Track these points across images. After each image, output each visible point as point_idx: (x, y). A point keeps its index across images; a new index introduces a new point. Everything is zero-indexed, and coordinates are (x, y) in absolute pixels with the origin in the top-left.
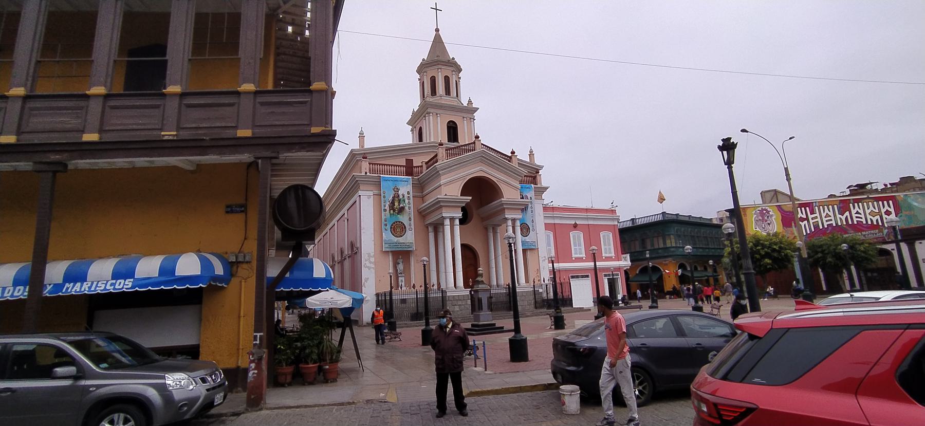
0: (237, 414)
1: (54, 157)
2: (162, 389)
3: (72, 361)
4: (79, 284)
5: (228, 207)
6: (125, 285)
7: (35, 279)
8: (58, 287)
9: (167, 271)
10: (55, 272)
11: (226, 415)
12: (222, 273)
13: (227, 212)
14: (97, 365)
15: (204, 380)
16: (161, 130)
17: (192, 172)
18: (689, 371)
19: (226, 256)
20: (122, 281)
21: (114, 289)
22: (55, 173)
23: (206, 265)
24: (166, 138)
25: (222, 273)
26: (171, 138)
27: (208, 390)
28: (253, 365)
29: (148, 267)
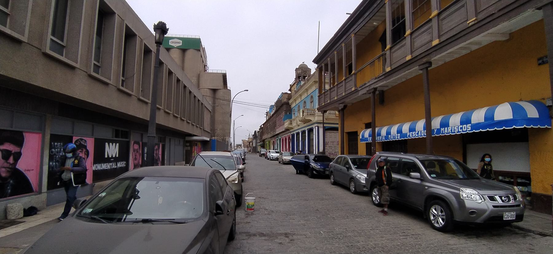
0: (543, 235)
1: (425, 60)
2: (457, 196)
3: (418, 170)
4: (446, 128)
5: (539, 60)
6: (467, 129)
7: (428, 126)
8: (439, 130)
9: (489, 117)
10: (436, 123)
11: (533, 232)
12: (537, 116)
13: (540, 64)
14: (430, 174)
15: (492, 198)
16: (467, 20)
17: (507, 41)
18: (8, 25)
19: (543, 101)
20: (465, 126)
21: (463, 131)
22: (427, 68)
23: (516, 109)
24: (470, 24)
25: (537, 116)
26: (473, 23)
27: (494, 206)
28: (70, 155)
29: (478, 116)
